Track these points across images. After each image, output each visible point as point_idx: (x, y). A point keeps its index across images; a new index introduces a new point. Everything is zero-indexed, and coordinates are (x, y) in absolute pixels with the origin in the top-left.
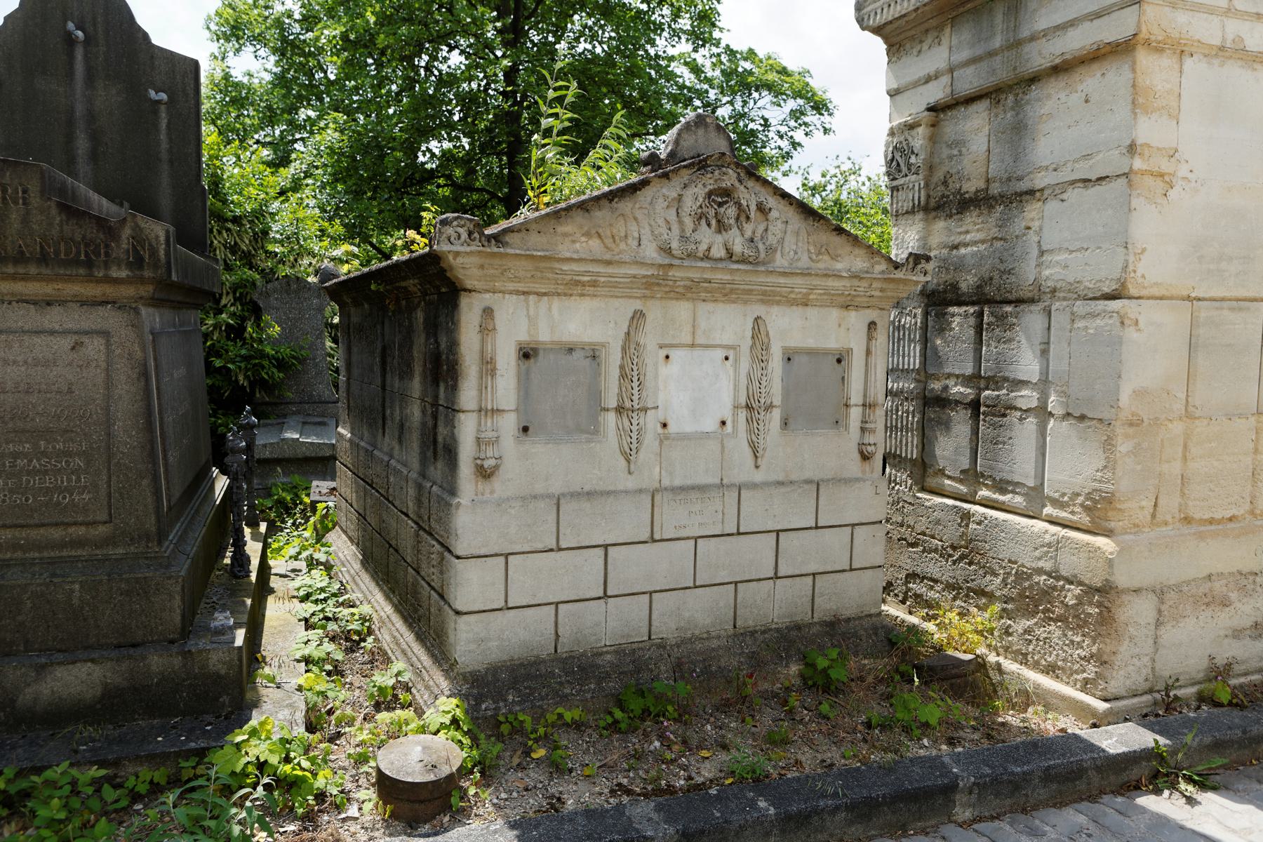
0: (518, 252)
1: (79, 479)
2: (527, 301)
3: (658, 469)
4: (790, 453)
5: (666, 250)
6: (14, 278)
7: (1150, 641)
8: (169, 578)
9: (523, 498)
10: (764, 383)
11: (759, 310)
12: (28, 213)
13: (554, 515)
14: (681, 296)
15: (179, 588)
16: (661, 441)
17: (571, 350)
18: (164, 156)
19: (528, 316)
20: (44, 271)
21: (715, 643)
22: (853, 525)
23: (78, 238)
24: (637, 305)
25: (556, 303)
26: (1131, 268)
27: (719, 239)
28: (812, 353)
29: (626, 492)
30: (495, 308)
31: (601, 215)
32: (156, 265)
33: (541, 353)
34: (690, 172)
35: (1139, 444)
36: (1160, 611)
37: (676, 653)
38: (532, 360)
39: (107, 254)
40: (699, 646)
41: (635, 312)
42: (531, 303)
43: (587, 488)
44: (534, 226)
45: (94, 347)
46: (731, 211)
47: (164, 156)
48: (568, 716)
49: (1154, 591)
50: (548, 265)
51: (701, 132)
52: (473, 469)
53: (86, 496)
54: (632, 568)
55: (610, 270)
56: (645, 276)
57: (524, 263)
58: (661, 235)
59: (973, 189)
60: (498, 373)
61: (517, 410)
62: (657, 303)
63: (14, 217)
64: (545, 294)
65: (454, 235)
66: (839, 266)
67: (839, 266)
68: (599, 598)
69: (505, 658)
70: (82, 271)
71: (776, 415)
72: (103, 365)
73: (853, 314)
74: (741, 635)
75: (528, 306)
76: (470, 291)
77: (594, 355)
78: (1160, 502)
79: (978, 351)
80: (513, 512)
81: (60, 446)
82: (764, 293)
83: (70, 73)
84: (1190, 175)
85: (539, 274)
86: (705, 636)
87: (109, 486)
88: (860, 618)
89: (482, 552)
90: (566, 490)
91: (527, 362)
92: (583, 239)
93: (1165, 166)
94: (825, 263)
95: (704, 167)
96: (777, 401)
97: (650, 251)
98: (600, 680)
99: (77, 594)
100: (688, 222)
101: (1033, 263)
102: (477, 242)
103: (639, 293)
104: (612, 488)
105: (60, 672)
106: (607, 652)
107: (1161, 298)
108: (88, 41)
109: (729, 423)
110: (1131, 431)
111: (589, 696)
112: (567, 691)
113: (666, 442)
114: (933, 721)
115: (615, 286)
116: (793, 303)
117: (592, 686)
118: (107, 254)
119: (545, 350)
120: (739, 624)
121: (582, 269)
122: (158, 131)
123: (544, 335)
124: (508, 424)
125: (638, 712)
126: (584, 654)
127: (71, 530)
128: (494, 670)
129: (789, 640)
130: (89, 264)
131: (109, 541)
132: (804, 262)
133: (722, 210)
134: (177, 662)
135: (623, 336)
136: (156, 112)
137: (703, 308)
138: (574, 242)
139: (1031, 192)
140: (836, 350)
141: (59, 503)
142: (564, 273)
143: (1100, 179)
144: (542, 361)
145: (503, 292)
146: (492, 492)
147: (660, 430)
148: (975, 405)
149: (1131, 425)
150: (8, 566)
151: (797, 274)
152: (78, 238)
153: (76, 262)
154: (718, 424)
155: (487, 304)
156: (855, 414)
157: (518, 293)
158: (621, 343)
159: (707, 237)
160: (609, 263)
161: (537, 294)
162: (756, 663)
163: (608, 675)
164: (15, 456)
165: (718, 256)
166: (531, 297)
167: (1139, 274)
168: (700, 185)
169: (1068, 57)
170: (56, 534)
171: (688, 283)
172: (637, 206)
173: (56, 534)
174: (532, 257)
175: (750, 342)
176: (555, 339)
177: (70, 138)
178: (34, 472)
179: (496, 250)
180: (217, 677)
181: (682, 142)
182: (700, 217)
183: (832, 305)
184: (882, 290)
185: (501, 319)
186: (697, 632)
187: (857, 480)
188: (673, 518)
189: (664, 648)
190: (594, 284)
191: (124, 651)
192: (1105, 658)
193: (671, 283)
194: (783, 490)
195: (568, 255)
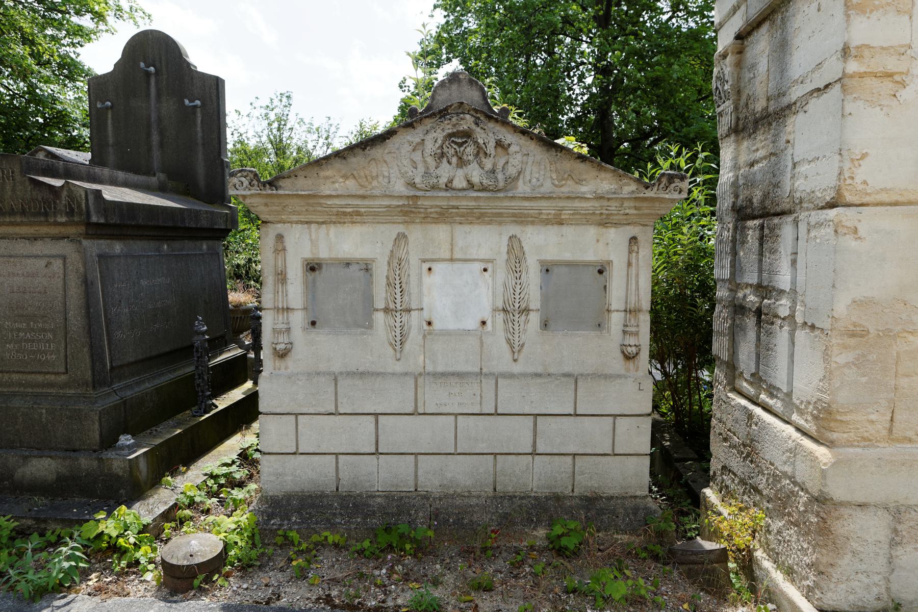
0: (287, 192)
1: (50, 347)
2: (309, 228)
3: (422, 358)
4: (543, 349)
5: (412, 185)
6: (12, 224)
7: (883, 560)
8: (92, 411)
9: (309, 374)
10: (518, 291)
11: (515, 230)
12: (14, 185)
13: (333, 388)
14: (436, 221)
15: (97, 418)
16: (424, 336)
17: (348, 264)
18: (200, 141)
20: (24, 220)
21: (474, 501)
22: (615, 416)
23: (40, 198)
24: (401, 228)
25: (333, 229)
26: (847, 175)
27: (460, 173)
28: (571, 265)
29: (393, 374)
30: (285, 234)
31: (356, 161)
32: (80, 214)
33: (324, 267)
34: (433, 120)
35: (864, 356)
36: (895, 531)
37: (438, 504)
38: (317, 272)
39: (55, 208)
40: (458, 502)
42: (313, 230)
43: (361, 369)
44: (301, 173)
45: (57, 264)
46: (470, 149)
47: (200, 141)
48: (331, 539)
49: (887, 509)
50: (316, 201)
51: (454, 87)
52: (272, 351)
53: (54, 357)
54: (398, 433)
55: (366, 202)
56: (398, 206)
57: (296, 201)
58: (406, 173)
59: (760, 109)
60: (289, 282)
61: (305, 309)
62: (418, 226)
63: (8, 188)
64: (323, 223)
65: (238, 183)
66: (584, 189)
67: (584, 189)
68: (373, 454)
69: (297, 489)
70: (42, 219)
71: (534, 319)
72: (62, 276)
73: (612, 231)
74: (499, 497)
75: (310, 232)
77: (367, 268)
78: (897, 417)
79: (760, 261)
80: (300, 383)
81: (40, 325)
82: (514, 215)
83: (148, 95)
85: (311, 209)
86: (466, 494)
87: (66, 351)
88: (624, 498)
89: (278, 411)
90: (344, 370)
91: (313, 274)
92: (341, 180)
93: (891, 64)
94: (569, 187)
95: (444, 116)
96: (535, 304)
97: (399, 187)
98: (365, 517)
99: (44, 416)
100: (431, 162)
101: (789, 175)
102: (256, 187)
103: (401, 219)
104: (382, 371)
105: (35, 462)
106: (379, 496)
107: (896, 204)
108: (157, 73)
109: (489, 323)
110: (852, 341)
111: (353, 526)
112: (338, 520)
113: (428, 337)
114: (617, 596)
115: (376, 214)
116: (547, 222)
117: (359, 520)
118: (55, 208)
119: (327, 264)
121: (343, 203)
122: (196, 125)
123: (324, 254)
124: (298, 319)
125: (384, 546)
126: (360, 495)
127: (47, 376)
128: (289, 497)
129: (545, 508)
130: (46, 214)
131: (65, 385)
132: (547, 187)
133: (462, 149)
134: (95, 463)
135: (388, 253)
136: (194, 113)
137: (460, 230)
138: (333, 182)
139: (789, 107)
140: (596, 262)
141: (40, 360)
142: (330, 206)
143: (827, 86)
144: (325, 273)
145: (291, 222)
146: (286, 368)
147: (426, 327)
148: (759, 312)
149: (853, 335)
150: (15, 396)
151: (540, 198)
152: (40, 198)
153: (39, 214)
154: (478, 324)
155: (279, 231)
156: (616, 319)
157: (302, 222)
158: (387, 258)
159: (445, 172)
160: (363, 197)
161: (317, 223)
162: (506, 521)
163: (374, 513)
164: (19, 330)
165: (460, 187)
166: (313, 225)
167: (858, 180)
168: (439, 131)
170: (40, 378)
171: (438, 210)
172: (386, 151)
173: (40, 378)
174: (302, 196)
175: (505, 256)
176: (333, 256)
177: (149, 135)
178: (27, 341)
179: (270, 192)
180: (118, 477)
181: (437, 97)
182: (441, 156)
183: (588, 223)
184: (636, 208)
185: (289, 242)
186: (459, 491)
187: (619, 376)
188: (434, 397)
189: (428, 499)
190: (358, 214)
191: (68, 454)
192: (822, 568)
193: (422, 210)
194: (539, 380)
195: (328, 192)
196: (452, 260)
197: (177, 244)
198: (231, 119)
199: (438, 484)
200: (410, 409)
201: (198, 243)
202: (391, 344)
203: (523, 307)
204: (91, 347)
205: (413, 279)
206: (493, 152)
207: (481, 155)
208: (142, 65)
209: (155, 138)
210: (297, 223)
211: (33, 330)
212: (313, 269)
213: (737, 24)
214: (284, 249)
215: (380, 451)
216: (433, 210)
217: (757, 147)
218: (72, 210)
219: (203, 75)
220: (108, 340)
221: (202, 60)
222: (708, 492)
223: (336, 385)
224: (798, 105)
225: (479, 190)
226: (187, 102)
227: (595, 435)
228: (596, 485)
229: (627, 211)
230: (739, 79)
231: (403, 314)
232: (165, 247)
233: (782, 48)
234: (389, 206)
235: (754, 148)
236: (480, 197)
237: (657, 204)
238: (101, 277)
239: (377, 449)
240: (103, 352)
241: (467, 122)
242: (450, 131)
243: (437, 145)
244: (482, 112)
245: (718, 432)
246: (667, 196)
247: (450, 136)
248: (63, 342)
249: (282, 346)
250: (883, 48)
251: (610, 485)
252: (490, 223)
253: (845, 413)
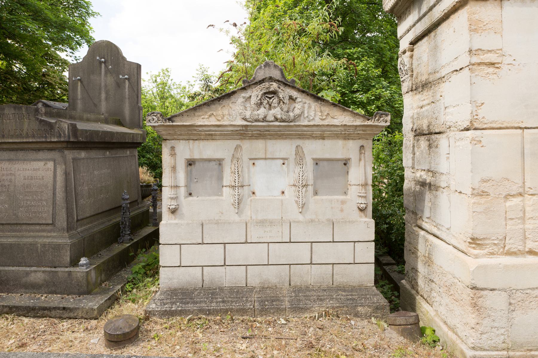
2: (189, 142)
11: (299, 142)
15: (69, 248)
18: (127, 97)
19: (190, 149)
22: (355, 242)
24: (238, 142)
38: (193, 166)
41: (237, 146)
44: (185, 114)
46: (275, 101)
54: (237, 254)
55: (220, 129)
59: (424, 80)
61: (186, 186)
64: (196, 140)
72: (53, 170)
76: (166, 140)
83: (100, 73)
84: (514, 62)
85: (190, 132)
96: (311, 182)
120: (292, 284)
121: (19, 141)
123: (196, 156)
124: (182, 191)
133: (271, 100)
136: (124, 82)
142: (200, 131)
143: (461, 69)
154: (280, 193)
165: (271, 120)
169: (446, 11)
171: (259, 132)
172: (231, 102)
175: (294, 156)
177: (100, 94)
179: (168, 124)
181: (258, 74)
182: (259, 104)
184: (363, 131)
185: (177, 150)
193: (250, 133)
196: (265, 159)
197: (114, 152)
198: (143, 84)
199: (258, 282)
200: (243, 241)
201: (125, 150)
202: (233, 205)
203: (304, 184)
204: (67, 209)
205: (245, 170)
206: (288, 102)
207: (281, 103)
208: (98, 58)
209: (103, 96)
210: (182, 139)
211: (35, 200)
212: (190, 165)
213: (411, 36)
214: (175, 154)
215: (226, 264)
216: (255, 132)
217: (424, 97)
218: (60, 135)
219: (131, 63)
220: (76, 204)
221: (130, 55)
222: (403, 282)
223: (202, 227)
224: (446, 78)
225: (280, 122)
226: (121, 77)
227: (344, 252)
228: (345, 281)
229: (359, 132)
230: (412, 64)
231: (240, 188)
232: (108, 153)
233: (435, 49)
234: (232, 131)
235: (422, 99)
236: (281, 125)
237: (374, 129)
238: (74, 170)
239: (225, 263)
240: (73, 211)
241: (274, 86)
242: (265, 91)
243: (258, 98)
244: (281, 82)
245: (408, 249)
246: (379, 124)
247: (265, 93)
248: (52, 206)
249: (174, 207)
250: (489, 51)
251: (353, 281)
252: (286, 139)
253: (481, 240)
